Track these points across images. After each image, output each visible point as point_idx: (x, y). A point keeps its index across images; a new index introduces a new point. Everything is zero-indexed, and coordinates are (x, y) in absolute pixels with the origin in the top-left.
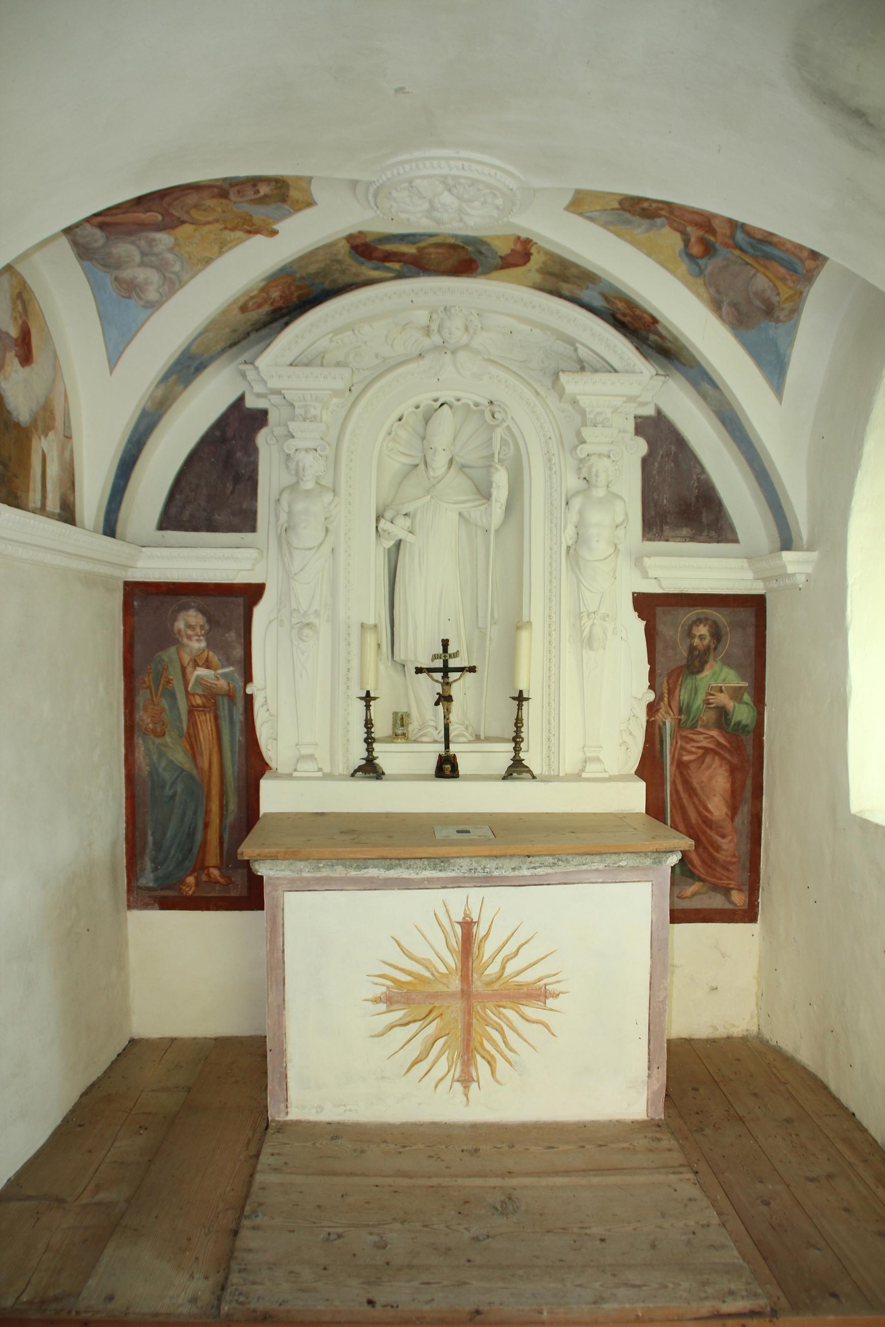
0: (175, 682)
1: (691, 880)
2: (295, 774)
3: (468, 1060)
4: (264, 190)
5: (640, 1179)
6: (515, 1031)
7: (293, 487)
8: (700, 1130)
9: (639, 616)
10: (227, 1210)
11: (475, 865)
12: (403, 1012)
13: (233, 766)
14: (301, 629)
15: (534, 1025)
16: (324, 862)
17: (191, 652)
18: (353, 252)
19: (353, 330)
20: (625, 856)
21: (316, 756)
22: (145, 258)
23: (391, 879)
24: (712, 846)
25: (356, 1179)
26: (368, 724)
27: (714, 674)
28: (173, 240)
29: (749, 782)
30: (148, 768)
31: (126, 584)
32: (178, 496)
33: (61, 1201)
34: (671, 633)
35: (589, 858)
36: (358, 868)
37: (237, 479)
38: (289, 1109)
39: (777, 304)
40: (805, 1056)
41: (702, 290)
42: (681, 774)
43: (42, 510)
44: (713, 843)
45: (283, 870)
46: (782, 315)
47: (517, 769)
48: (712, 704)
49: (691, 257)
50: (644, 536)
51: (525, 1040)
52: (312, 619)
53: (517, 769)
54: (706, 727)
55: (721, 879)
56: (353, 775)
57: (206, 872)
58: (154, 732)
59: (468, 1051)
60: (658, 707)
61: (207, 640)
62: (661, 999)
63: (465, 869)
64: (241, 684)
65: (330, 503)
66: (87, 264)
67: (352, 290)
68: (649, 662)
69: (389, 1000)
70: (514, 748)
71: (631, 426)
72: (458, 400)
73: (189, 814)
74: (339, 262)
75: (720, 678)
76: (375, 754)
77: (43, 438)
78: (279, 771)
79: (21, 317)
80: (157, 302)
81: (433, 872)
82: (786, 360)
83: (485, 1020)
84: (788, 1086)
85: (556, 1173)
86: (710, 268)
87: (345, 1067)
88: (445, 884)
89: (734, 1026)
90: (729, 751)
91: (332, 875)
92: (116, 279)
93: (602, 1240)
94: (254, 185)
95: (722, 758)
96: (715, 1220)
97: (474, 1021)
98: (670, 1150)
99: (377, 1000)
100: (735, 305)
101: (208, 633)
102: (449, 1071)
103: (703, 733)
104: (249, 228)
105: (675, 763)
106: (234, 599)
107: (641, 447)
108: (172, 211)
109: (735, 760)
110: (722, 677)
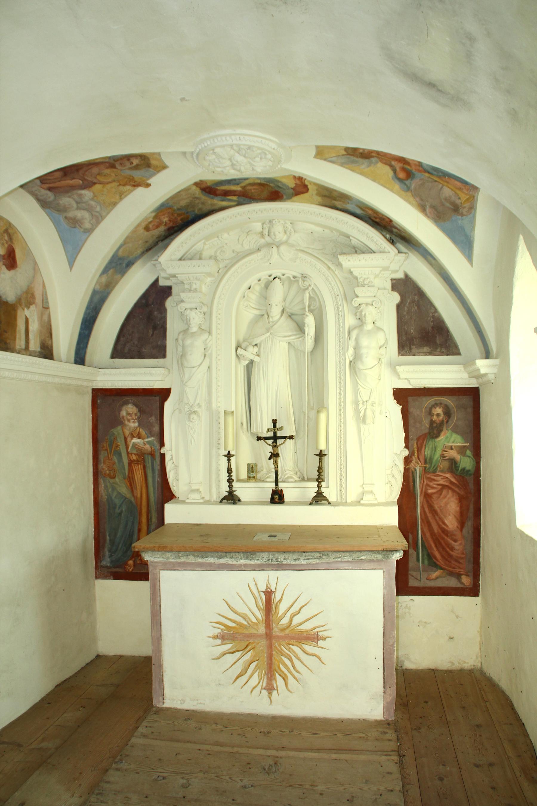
0: (121, 447)
1: (434, 569)
2: (187, 501)
3: (271, 676)
4: (135, 162)
5: (363, 757)
6: (300, 660)
7: (185, 331)
8: (418, 729)
9: (398, 403)
10: (110, 758)
11: (271, 557)
12: (231, 645)
13: (154, 496)
14: (190, 414)
15: (311, 657)
16: (182, 553)
17: (130, 429)
18: (204, 192)
19: (218, 237)
20: (364, 553)
21: (201, 490)
22: (79, 205)
23: (223, 564)
24: (448, 547)
25: (189, 745)
26: (229, 471)
27: (447, 437)
28: (92, 194)
29: (472, 507)
30: (106, 496)
31: (94, 390)
32: (122, 339)
33: (20, 745)
34: (418, 413)
35: (342, 554)
36: (202, 557)
37: (155, 328)
38: (165, 701)
39: (460, 204)
40: (504, 684)
41: (411, 199)
42: (427, 501)
43: (26, 351)
44: (448, 545)
45: (159, 557)
46: (464, 211)
47: (319, 498)
48: (446, 457)
49: (400, 180)
50: (399, 353)
51: (306, 666)
52: (196, 409)
53: (319, 498)
54: (442, 471)
55: (454, 568)
56: (221, 502)
57: (139, 558)
58: (109, 475)
59: (270, 671)
60: (411, 459)
61: (139, 422)
62: (391, 644)
63: (266, 559)
64: (158, 447)
65: (206, 340)
66: (47, 210)
67: (213, 213)
68: (405, 432)
69: (223, 638)
70: (318, 486)
71: (389, 285)
72: (284, 275)
73: (130, 524)
74: (197, 198)
75: (450, 441)
76: (234, 489)
77: (26, 309)
78: (180, 499)
79: (7, 243)
80: (91, 229)
81: (246, 560)
82: (472, 239)
83: (281, 652)
84: (488, 703)
85: (311, 750)
86: (413, 186)
87: (198, 677)
88: (255, 568)
89: (465, 662)
90: (458, 487)
91: (187, 561)
92: (66, 217)
93: (321, 794)
94: (129, 160)
95: (454, 491)
96: (398, 788)
97: (274, 652)
98: (390, 740)
99: (215, 637)
100: (433, 207)
101: (139, 418)
102: (259, 683)
103: (441, 476)
104: (134, 184)
105: (423, 494)
106: (154, 397)
107: (396, 298)
108: (86, 178)
109: (462, 493)
110: (452, 440)
